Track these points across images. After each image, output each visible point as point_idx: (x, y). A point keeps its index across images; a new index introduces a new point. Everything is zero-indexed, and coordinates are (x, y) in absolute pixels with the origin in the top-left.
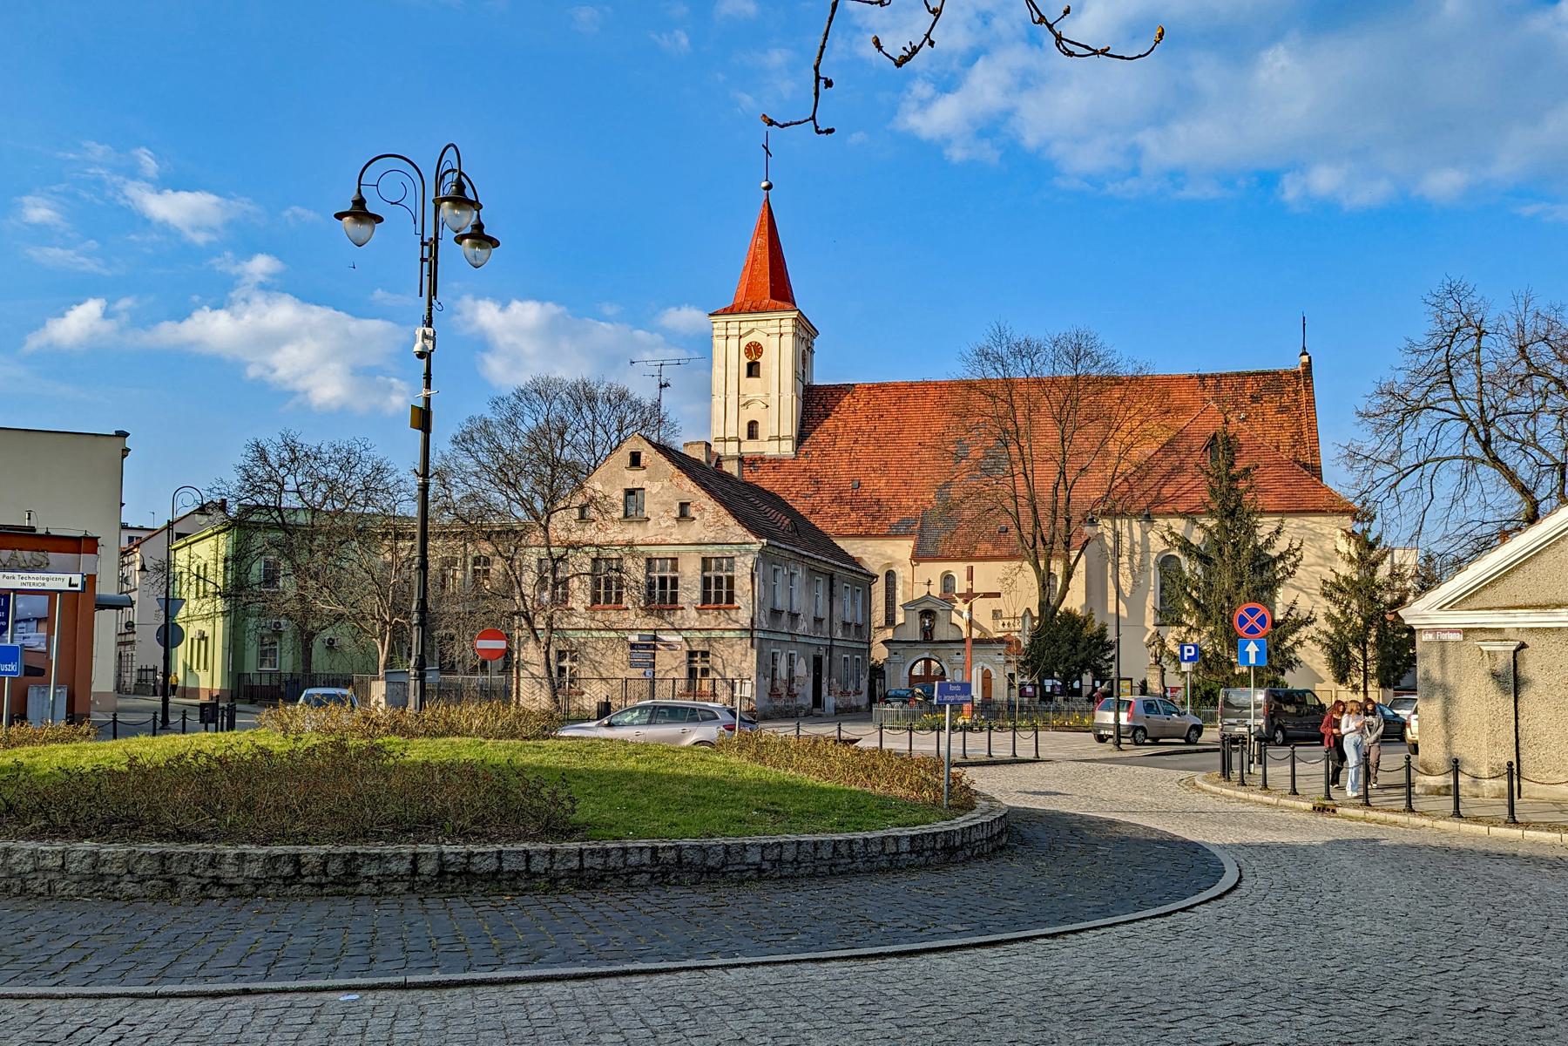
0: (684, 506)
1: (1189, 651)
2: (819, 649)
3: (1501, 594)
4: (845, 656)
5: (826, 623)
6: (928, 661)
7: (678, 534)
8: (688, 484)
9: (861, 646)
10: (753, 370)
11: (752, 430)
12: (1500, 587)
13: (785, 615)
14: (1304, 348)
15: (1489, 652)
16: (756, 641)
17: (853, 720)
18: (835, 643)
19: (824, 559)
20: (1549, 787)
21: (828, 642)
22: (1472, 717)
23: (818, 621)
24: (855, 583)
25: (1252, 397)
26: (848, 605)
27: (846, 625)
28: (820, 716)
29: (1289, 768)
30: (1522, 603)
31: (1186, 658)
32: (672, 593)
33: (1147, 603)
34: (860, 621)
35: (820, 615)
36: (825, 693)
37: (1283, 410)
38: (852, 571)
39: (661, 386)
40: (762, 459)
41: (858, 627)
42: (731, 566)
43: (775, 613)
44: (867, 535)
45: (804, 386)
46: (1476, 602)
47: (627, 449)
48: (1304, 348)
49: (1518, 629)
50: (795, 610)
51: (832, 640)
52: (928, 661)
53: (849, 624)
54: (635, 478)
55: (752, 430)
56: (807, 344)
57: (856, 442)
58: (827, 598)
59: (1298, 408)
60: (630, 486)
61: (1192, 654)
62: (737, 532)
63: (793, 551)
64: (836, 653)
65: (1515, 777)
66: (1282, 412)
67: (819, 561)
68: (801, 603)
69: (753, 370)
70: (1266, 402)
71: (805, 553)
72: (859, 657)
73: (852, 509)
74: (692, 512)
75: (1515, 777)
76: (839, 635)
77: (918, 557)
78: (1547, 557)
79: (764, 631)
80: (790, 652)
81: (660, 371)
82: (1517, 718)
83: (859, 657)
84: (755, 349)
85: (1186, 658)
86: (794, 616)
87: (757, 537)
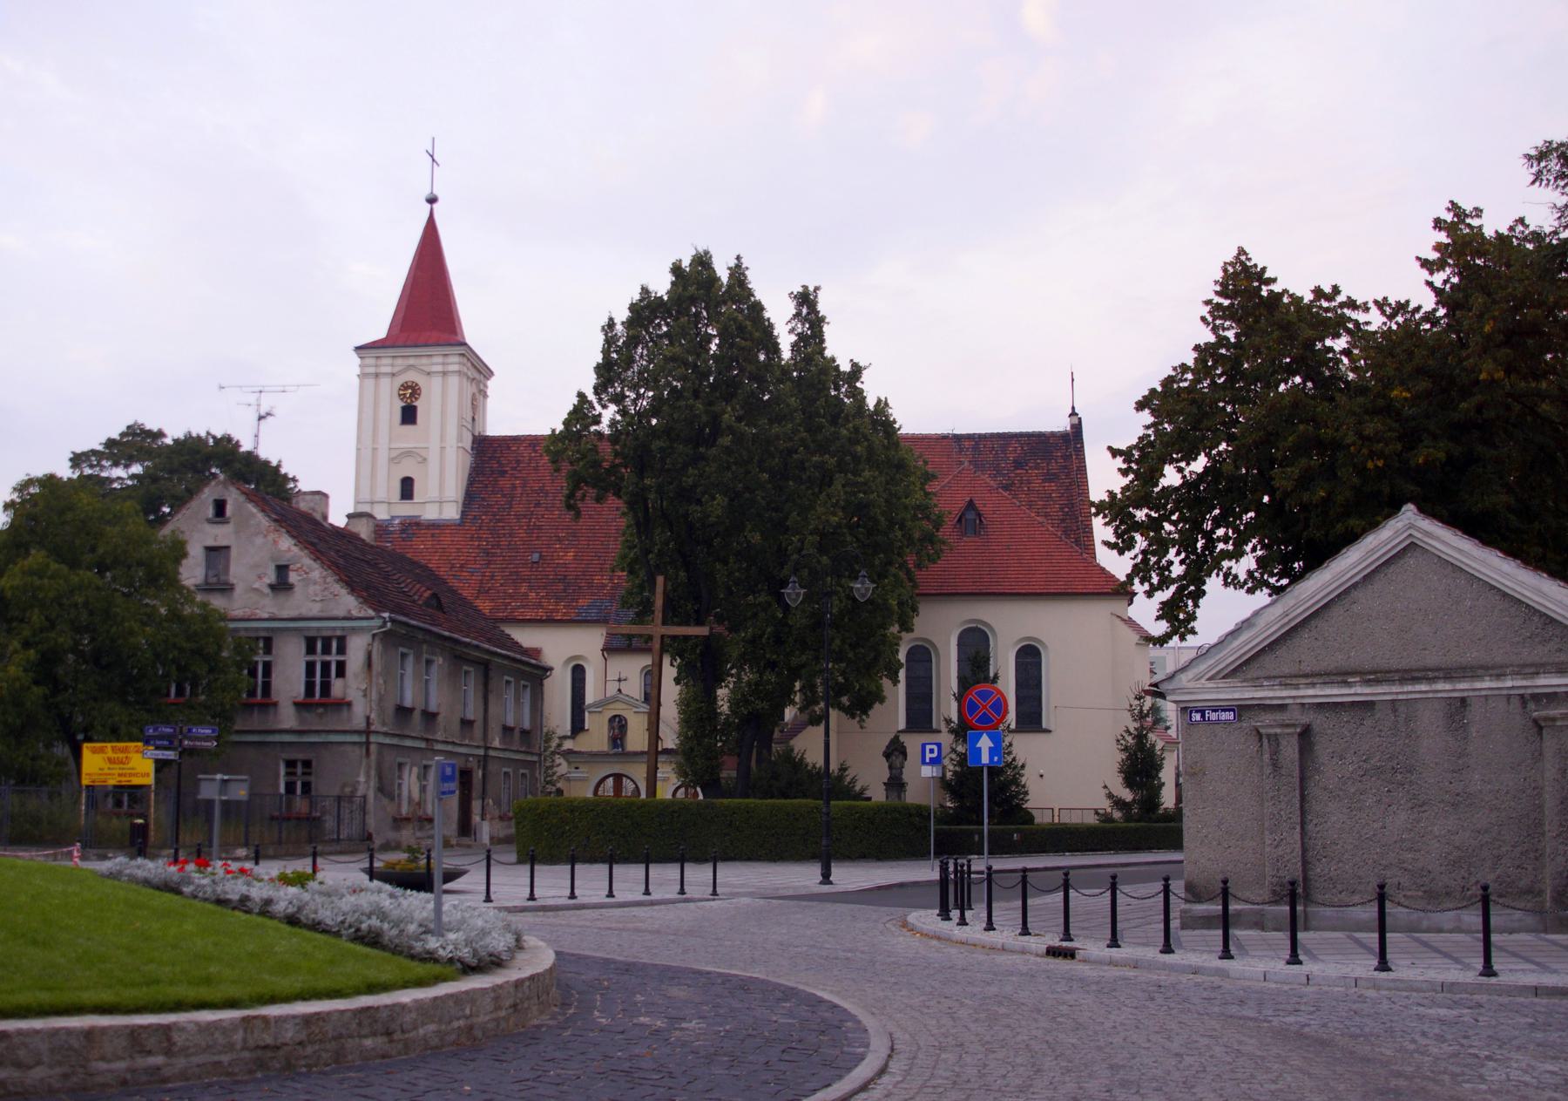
0: (282, 570)
1: (932, 751)
2: (467, 761)
3: (1283, 662)
4: (505, 769)
5: (478, 730)
6: (618, 778)
7: (268, 606)
8: (286, 543)
9: (529, 758)
10: (409, 415)
11: (407, 488)
12: (1282, 651)
13: (417, 715)
14: (1073, 408)
15: (1268, 736)
16: (373, 748)
17: (464, 855)
18: (492, 753)
19: (475, 642)
20: (1141, 901)
21: (481, 752)
22: (1249, 823)
23: (466, 724)
24: (519, 675)
25: (1015, 461)
26: (511, 704)
27: (507, 730)
28: (469, 846)
29: (1019, 903)
30: (1308, 670)
31: (928, 760)
32: (263, 682)
33: (660, 615)
34: (527, 725)
35: (470, 716)
36: (476, 818)
37: (1050, 477)
38: (514, 660)
39: (261, 418)
40: (418, 524)
41: (524, 733)
42: (342, 650)
43: (403, 712)
44: (549, 621)
45: (473, 435)
46: (1253, 672)
47: (208, 495)
48: (1073, 408)
49: (1303, 704)
50: (433, 708)
51: (487, 748)
52: (618, 778)
53: (411, 710)
54: (219, 535)
55: (407, 488)
56: (478, 386)
57: (538, 505)
58: (480, 695)
59: (1068, 475)
60: (211, 543)
61: (935, 755)
62: (348, 603)
63: (430, 632)
64: (492, 767)
65: (271, 738)
66: (1050, 481)
67: (467, 645)
68: (438, 698)
69: (409, 415)
70: (1031, 468)
71: (447, 634)
72: (509, 770)
73: (531, 589)
74: (293, 577)
75: (271, 738)
76: (497, 743)
77: (610, 649)
78: (1337, 611)
79: (386, 734)
80: (425, 762)
81: (258, 399)
82: (1303, 824)
83: (509, 770)
84: (410, 393)
85: (928, 760)
86: (430, 717)
87: (374, 610)
